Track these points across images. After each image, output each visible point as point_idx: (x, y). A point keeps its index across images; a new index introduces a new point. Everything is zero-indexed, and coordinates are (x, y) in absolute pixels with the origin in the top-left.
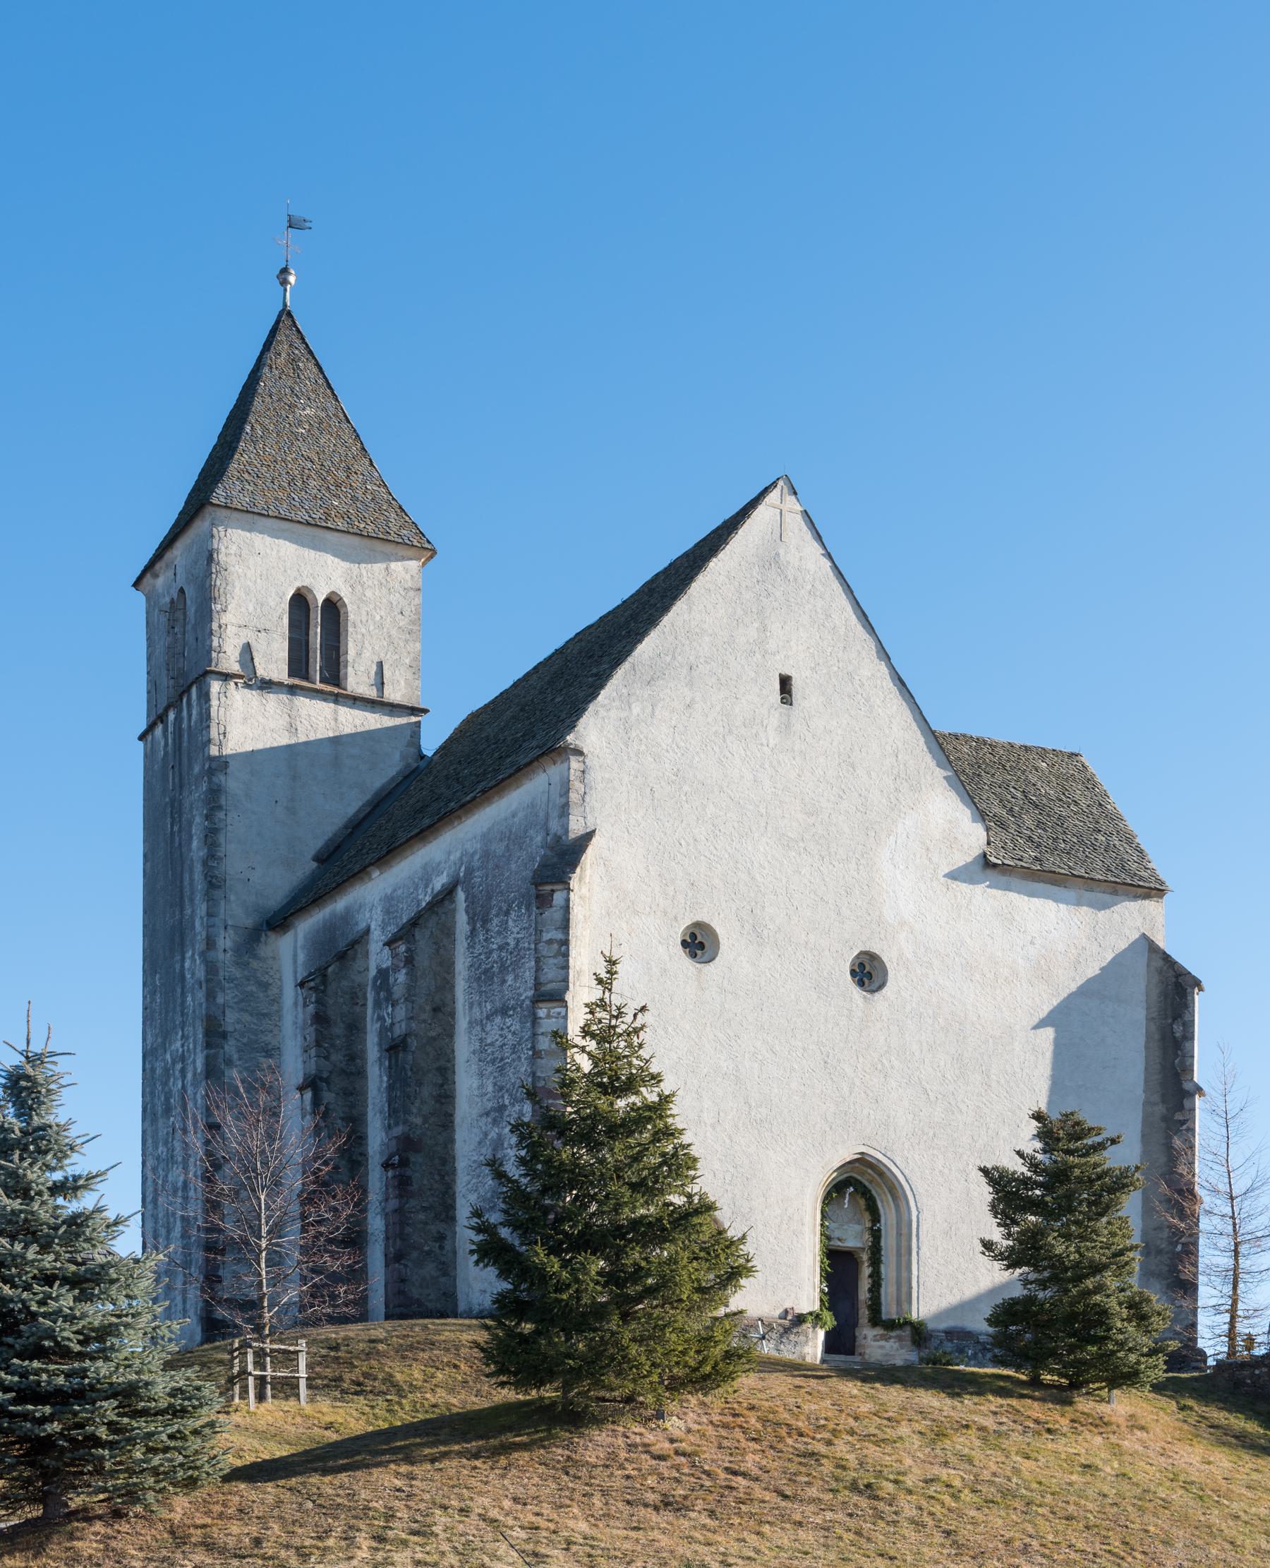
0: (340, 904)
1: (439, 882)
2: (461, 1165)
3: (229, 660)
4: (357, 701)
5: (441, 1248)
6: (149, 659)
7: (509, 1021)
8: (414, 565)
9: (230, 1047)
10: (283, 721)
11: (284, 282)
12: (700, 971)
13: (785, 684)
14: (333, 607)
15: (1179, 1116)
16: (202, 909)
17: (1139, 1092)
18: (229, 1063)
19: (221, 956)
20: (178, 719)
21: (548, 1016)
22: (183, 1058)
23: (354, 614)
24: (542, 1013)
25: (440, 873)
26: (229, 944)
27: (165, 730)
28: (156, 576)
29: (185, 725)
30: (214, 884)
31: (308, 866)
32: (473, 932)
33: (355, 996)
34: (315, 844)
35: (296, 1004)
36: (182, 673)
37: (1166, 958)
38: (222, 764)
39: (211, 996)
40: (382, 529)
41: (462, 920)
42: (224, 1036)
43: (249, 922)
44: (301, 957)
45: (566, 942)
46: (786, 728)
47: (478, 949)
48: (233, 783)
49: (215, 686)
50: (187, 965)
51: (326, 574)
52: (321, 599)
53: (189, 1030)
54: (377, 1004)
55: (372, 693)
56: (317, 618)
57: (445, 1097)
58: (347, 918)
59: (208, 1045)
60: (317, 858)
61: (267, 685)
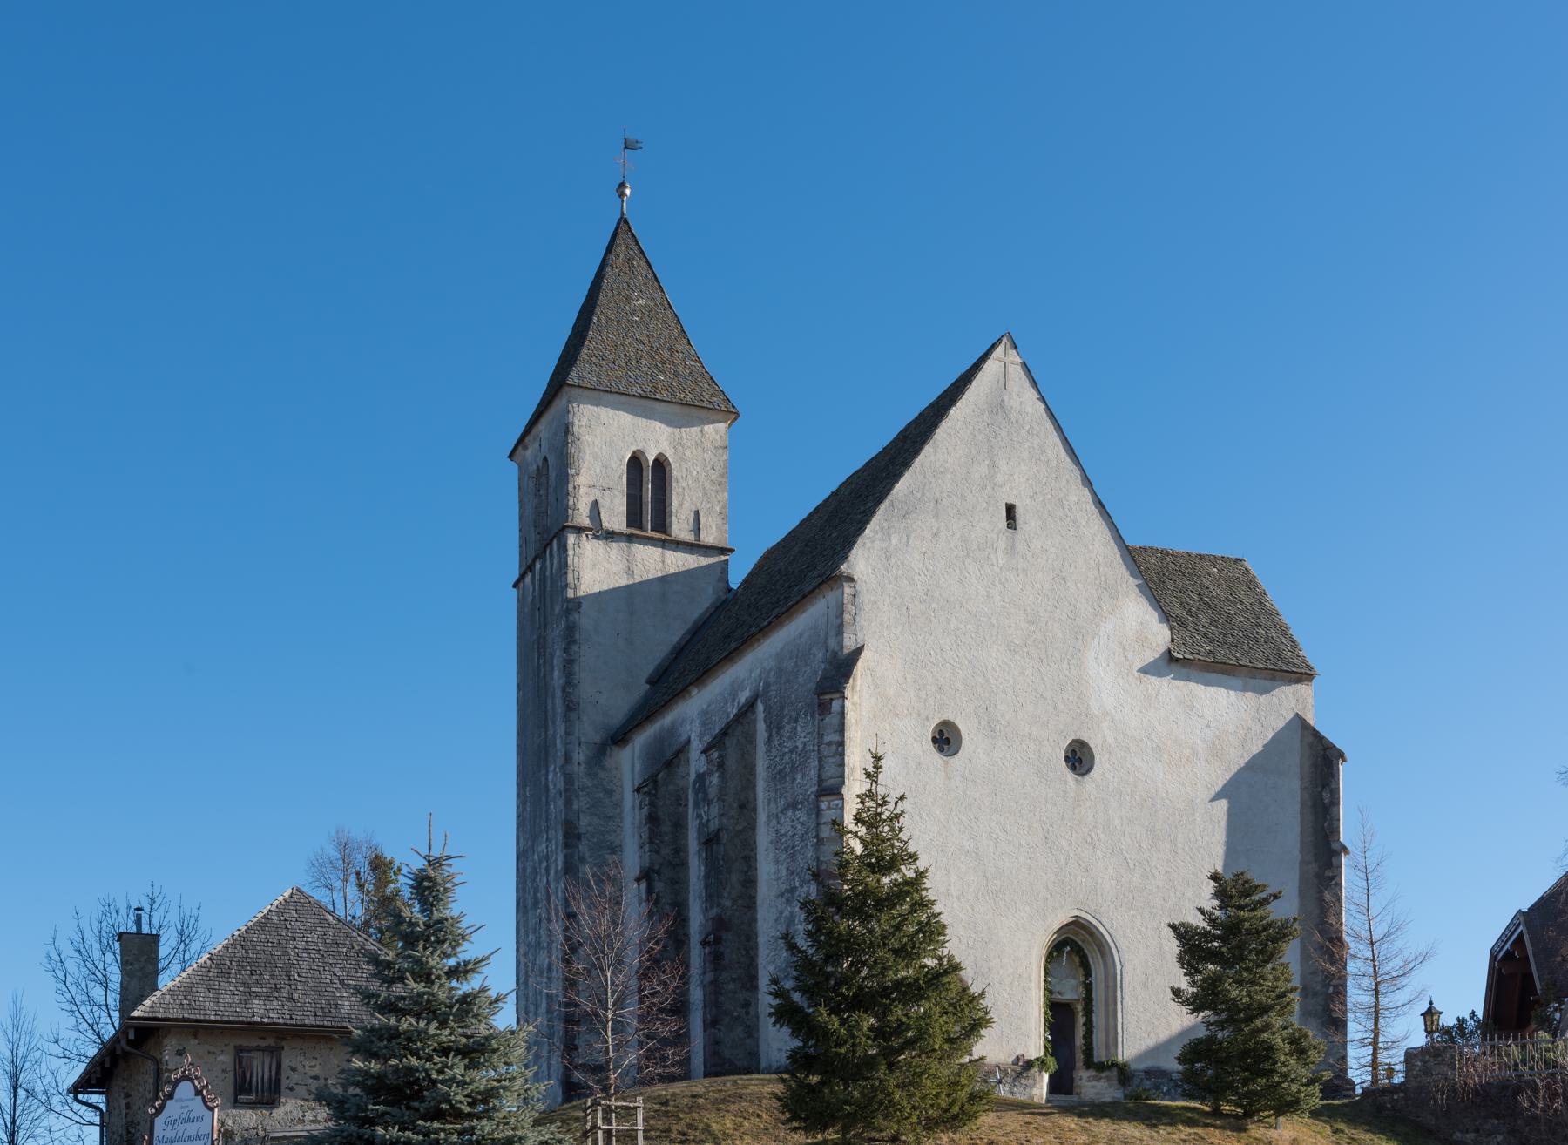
1: (744, 697)
2: (762, 940)
3: (582, 517)
5: (747, 1013)
7: (798, 814)
9: (583, 847)
10: (622, 566)
11: (622, 195)
12: (946, 763)
13: (1010, 510)
14: (661, 465)
15: (1328, 873)
16: (561, 729)
18: (582, 860)
19: (576, 768)
21: (829, 808)
22: (547, 858)
23: (677, 470)
24: (824, 805)
26: (582, 758)
28: (526, 448)
30: (571, 707)
32: (770, 740)
33: (679, 799)
34: (648, 669)
36: (546, 529)
37: (1316, 734)
38: (577, 604)
39: (568, 803)
40: (693, 397)
41: (761, 727)
42: (579, 837)
43: (597, 738)
44: (638, 767)
45: (842, 743)
46: (1011, 549)
48: (584, 620)
49: (571, 539)
51: (655, 438)
54: (696, 804)
55: (690, 537)
56: (648, 475)
57: (750, 882)
58: (672, 731)
59: (567, 846)
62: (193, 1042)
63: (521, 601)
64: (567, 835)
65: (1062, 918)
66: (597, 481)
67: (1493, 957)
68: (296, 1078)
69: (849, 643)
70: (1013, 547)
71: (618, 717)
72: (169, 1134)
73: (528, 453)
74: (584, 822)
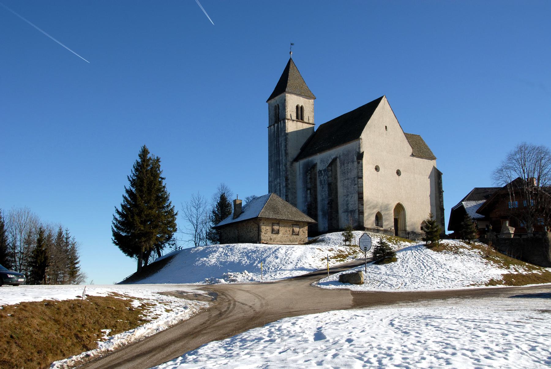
0: (310, 159)
3: (289, 117)
4: (306, 123)
6: (269, 114)
8: (313, 100)
9: (289, 182)
10: (295, 127)
14: (302, 107)
20: (278, 126)
27: (274, 127)
30: (286, 154)
31: (299, 151)
33: (315, 175)
34: (300, 147)
36: (278, 117)
37: (437, 170)
38: (288, 134)
39: (286, 173)
40: (308, 95)
43: (291, 160)
48: (289, 137)
49: (286, 121)
54: (319, 176)
56: (300, 109)
57: (337, 193)
58: (312, 161)
61: (293, 120)
63: (270, 131)
65: (397, 203)
66: (291, 111)
67: (452, 209)
69: (362, 151)
71: (295, 156)
73: (273, 101)
74: (289, 176)
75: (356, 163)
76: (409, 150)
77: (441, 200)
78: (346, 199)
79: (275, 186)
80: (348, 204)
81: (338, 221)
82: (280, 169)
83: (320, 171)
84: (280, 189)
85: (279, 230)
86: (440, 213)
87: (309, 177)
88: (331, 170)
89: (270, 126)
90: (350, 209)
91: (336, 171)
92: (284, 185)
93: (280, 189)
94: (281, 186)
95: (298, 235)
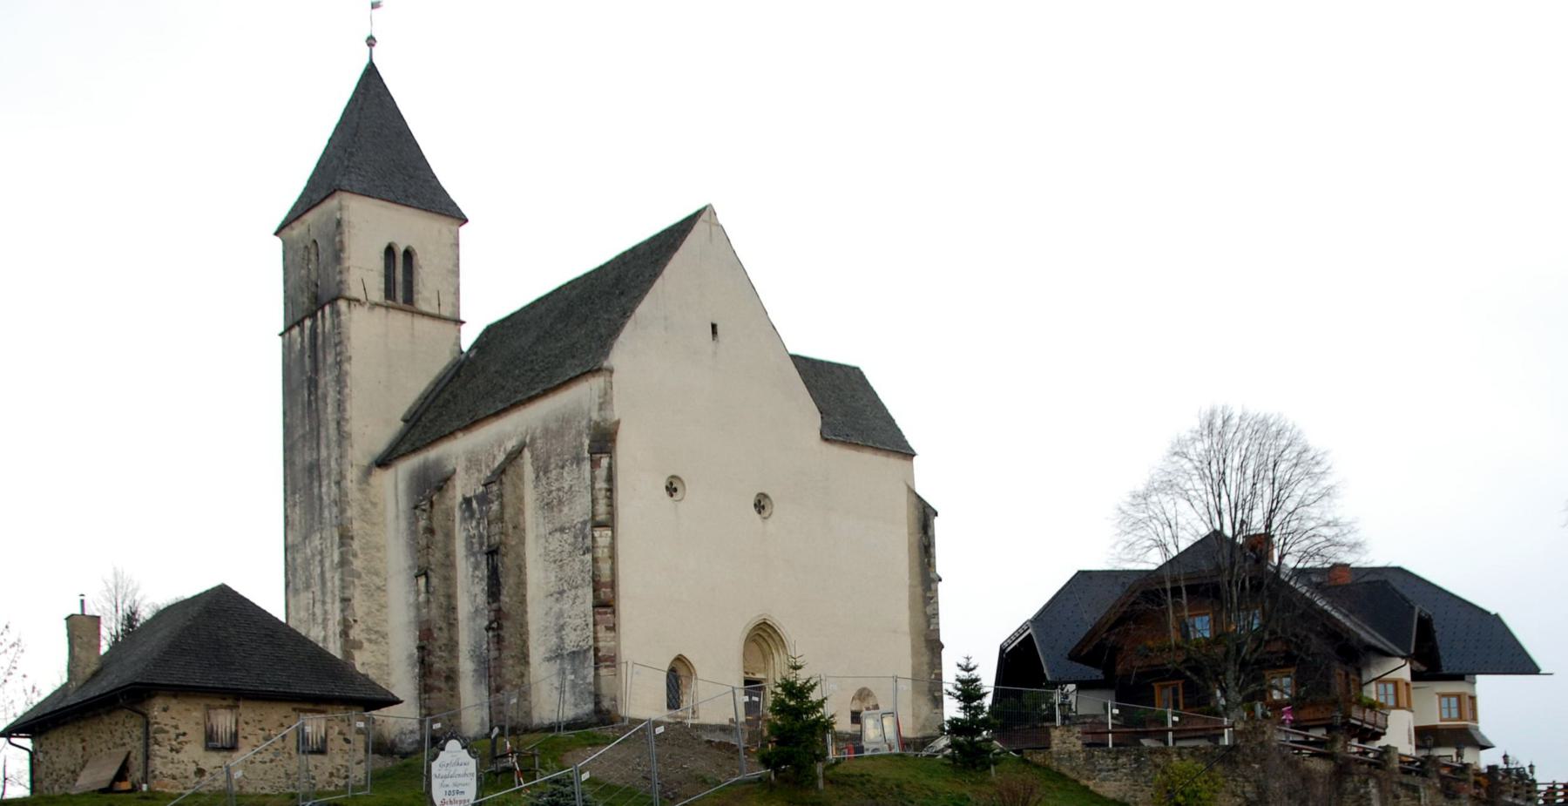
0: (432, 454)
1: (510, 445)
3: (355, 291)
9: (356, 545)
13: (714, 327)
14: (408, 254)
16: (335, 453)
17: (907, 582)
22: (321, 553)
23: (420, 259)
24: (597, 534)
25: (510, 438)
27: (302, 331)
29: (319, 330)
30: (343, 437)
31: (397, 425)
33: (449, 516)
35: (397, 517)
43: (366, 462)
47: (541, 489)
49: (342, 305)
50: (324, 489)
52: (402, 249)
53: (326, 533)
54: (464, 520)
58: (438, 463)
59: (342, 544)
60: (405, 420)
62: (174, 701)
63: (287, 349)
64: (342, 537)
66: (363, 271)
67: (1002, 650)
68: (248, 729)
70: (715, 353)
71: (380, 445)
72: (443, 772)
73: (298, 230)
75: (587, 466)
76: (811, 418)
77: (929, 610)
78: (556, 607)
79: (307, 562)
80: (562, 628)
81: (524, 695)
82: (321, 499)
83: (467, 501)
84: (323, 573)
85: (235, 735)
86: (925, 659)
87: (422, 523)
88: (501, 496)
89: (288, 329)
90: (570, 646)
91: (521, 499)
92: (336, 558)
93: (323, 573)
94: (327, 564)
95: (321, 751)
